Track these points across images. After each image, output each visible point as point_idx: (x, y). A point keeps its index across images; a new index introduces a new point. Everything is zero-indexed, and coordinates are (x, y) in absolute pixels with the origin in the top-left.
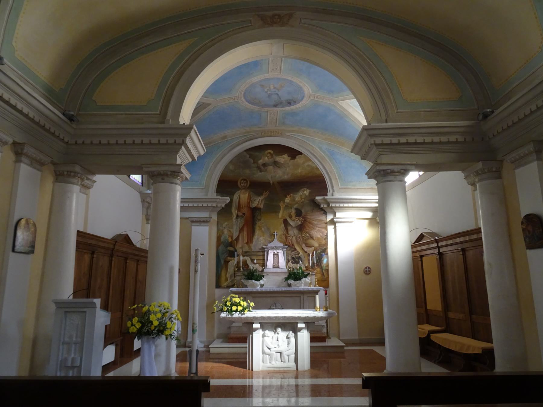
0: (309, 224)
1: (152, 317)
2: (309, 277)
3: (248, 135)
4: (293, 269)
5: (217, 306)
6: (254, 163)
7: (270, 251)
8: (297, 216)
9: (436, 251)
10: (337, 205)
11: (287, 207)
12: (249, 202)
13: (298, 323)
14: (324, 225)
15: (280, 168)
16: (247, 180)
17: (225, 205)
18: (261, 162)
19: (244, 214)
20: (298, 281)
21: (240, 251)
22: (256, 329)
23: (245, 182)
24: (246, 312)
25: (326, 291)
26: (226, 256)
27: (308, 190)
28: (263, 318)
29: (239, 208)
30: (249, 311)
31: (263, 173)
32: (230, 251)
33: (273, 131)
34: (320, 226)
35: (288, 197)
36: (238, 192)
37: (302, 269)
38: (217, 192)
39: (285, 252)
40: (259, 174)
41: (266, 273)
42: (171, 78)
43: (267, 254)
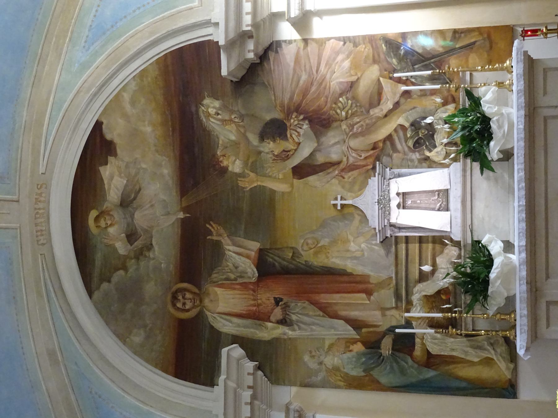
2: (480, 92)
6: (125, 268)
7: (393, 220)
14: (312, 48)
17: (252, 359)
18: (122, 247)
19: (277, 301)
20: (494, 126)
27: (207, 101)
34: (314, 62)
36: (210, 319)
37: (454, 116)
39: (396, 171)
41: (464, 232)
43: (401, 228)
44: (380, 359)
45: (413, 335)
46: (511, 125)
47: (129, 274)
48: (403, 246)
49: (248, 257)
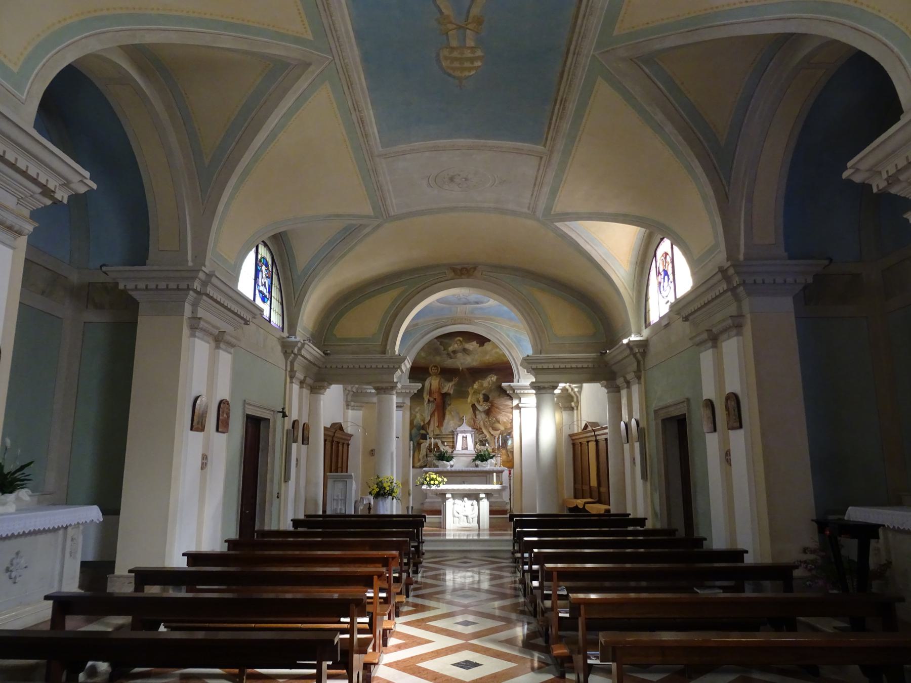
0: (496, 409)
1: (385, 485)
2: (494, 458)
4: (481, 452)
5: (419, 481)
6: (444, 350)
7: (459, 434)
8: (484, 401)
9: (594, 438)
10: (522, 392)
11: (476, 392)
12: (440, 388)
13: (480, 494)
14: (510, 410)
16: (439, 367)
17: (417, 391)
18: (451, 349)
19: (435, 399)
20: (485, 462)
21: (431, 434)
22: (449, 498)
24: (441, 485)
25: (510, 471)
26: (419, 438)
27: (495, 377)
28: (454, 490)
29: (430, 393)
30: (443, 484)
32: (422, 434)
34: (506, 410)
36: (429, 378)
37: (488, 451)
38: (409, 378)
39: (473, 435)
41: (456, 454)
42: (388, 318)
43: (457, 436)
44: (419, 430)
45: (427, 439)
46: (484, 467)
47: (442, 351)
48: (451, 437)
49: (448, 390)
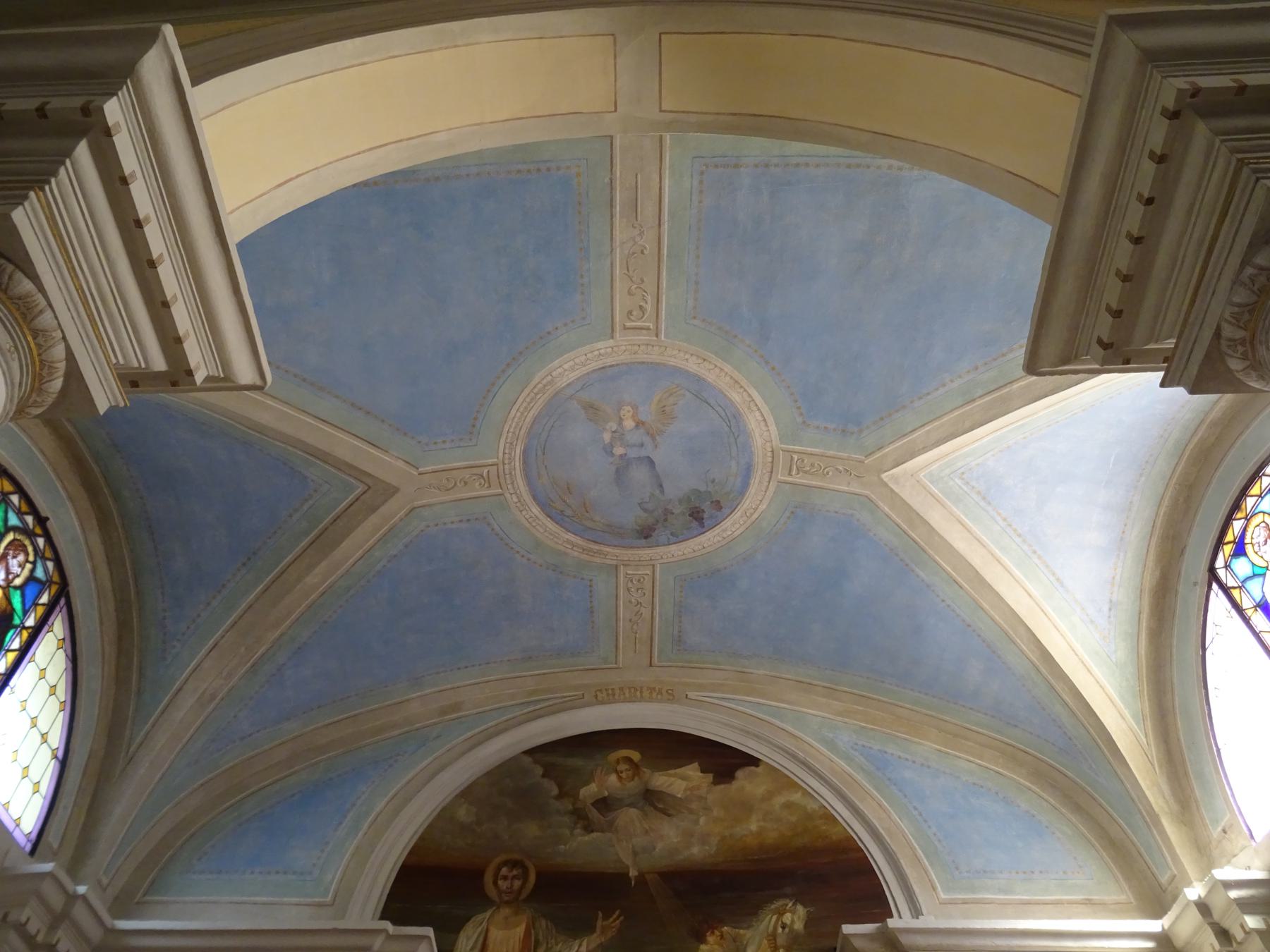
3: (548, 699)
6: (560, 796)
15: (669, 815)
18: (590, 791)
23: (515, 872)
27: (801, 910)
31: (595, 835)
33: (641, 688)
35: (711, 939)
36: (480, 917)
40: (580, 838)
